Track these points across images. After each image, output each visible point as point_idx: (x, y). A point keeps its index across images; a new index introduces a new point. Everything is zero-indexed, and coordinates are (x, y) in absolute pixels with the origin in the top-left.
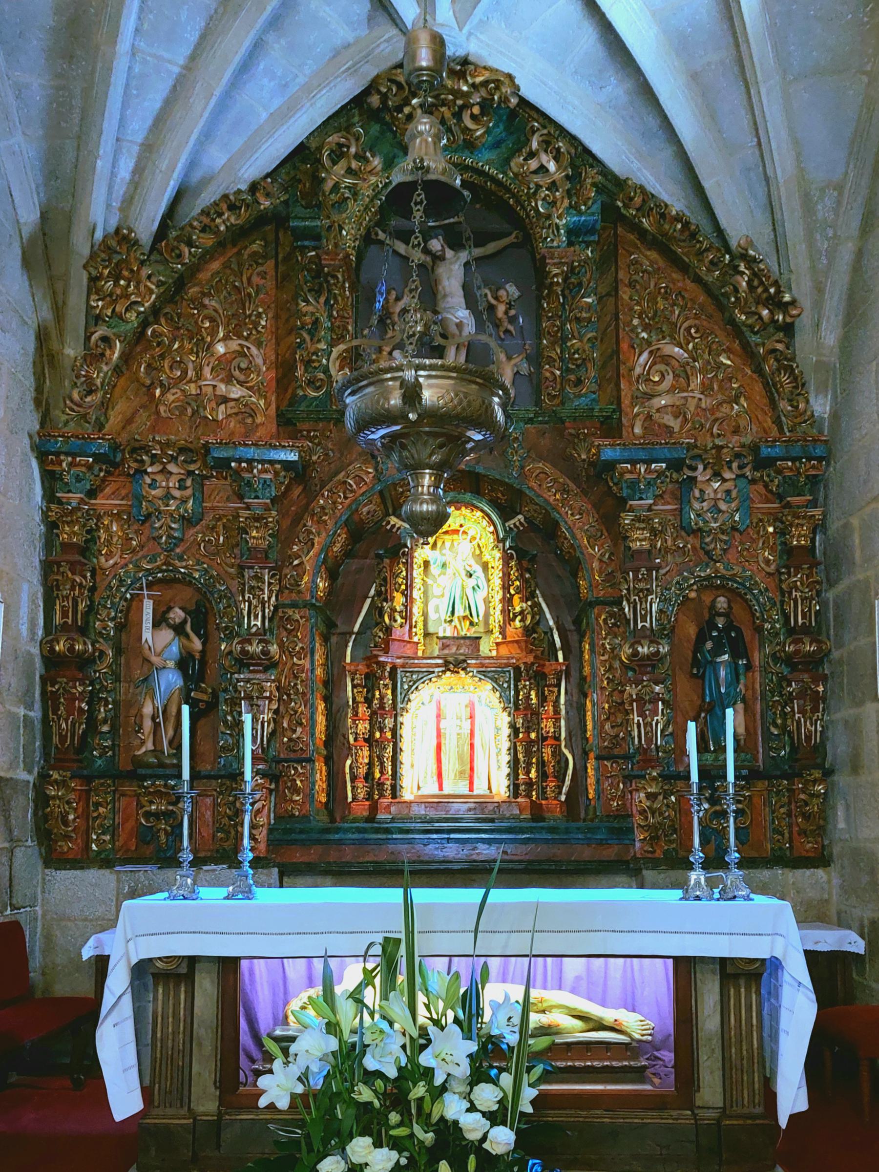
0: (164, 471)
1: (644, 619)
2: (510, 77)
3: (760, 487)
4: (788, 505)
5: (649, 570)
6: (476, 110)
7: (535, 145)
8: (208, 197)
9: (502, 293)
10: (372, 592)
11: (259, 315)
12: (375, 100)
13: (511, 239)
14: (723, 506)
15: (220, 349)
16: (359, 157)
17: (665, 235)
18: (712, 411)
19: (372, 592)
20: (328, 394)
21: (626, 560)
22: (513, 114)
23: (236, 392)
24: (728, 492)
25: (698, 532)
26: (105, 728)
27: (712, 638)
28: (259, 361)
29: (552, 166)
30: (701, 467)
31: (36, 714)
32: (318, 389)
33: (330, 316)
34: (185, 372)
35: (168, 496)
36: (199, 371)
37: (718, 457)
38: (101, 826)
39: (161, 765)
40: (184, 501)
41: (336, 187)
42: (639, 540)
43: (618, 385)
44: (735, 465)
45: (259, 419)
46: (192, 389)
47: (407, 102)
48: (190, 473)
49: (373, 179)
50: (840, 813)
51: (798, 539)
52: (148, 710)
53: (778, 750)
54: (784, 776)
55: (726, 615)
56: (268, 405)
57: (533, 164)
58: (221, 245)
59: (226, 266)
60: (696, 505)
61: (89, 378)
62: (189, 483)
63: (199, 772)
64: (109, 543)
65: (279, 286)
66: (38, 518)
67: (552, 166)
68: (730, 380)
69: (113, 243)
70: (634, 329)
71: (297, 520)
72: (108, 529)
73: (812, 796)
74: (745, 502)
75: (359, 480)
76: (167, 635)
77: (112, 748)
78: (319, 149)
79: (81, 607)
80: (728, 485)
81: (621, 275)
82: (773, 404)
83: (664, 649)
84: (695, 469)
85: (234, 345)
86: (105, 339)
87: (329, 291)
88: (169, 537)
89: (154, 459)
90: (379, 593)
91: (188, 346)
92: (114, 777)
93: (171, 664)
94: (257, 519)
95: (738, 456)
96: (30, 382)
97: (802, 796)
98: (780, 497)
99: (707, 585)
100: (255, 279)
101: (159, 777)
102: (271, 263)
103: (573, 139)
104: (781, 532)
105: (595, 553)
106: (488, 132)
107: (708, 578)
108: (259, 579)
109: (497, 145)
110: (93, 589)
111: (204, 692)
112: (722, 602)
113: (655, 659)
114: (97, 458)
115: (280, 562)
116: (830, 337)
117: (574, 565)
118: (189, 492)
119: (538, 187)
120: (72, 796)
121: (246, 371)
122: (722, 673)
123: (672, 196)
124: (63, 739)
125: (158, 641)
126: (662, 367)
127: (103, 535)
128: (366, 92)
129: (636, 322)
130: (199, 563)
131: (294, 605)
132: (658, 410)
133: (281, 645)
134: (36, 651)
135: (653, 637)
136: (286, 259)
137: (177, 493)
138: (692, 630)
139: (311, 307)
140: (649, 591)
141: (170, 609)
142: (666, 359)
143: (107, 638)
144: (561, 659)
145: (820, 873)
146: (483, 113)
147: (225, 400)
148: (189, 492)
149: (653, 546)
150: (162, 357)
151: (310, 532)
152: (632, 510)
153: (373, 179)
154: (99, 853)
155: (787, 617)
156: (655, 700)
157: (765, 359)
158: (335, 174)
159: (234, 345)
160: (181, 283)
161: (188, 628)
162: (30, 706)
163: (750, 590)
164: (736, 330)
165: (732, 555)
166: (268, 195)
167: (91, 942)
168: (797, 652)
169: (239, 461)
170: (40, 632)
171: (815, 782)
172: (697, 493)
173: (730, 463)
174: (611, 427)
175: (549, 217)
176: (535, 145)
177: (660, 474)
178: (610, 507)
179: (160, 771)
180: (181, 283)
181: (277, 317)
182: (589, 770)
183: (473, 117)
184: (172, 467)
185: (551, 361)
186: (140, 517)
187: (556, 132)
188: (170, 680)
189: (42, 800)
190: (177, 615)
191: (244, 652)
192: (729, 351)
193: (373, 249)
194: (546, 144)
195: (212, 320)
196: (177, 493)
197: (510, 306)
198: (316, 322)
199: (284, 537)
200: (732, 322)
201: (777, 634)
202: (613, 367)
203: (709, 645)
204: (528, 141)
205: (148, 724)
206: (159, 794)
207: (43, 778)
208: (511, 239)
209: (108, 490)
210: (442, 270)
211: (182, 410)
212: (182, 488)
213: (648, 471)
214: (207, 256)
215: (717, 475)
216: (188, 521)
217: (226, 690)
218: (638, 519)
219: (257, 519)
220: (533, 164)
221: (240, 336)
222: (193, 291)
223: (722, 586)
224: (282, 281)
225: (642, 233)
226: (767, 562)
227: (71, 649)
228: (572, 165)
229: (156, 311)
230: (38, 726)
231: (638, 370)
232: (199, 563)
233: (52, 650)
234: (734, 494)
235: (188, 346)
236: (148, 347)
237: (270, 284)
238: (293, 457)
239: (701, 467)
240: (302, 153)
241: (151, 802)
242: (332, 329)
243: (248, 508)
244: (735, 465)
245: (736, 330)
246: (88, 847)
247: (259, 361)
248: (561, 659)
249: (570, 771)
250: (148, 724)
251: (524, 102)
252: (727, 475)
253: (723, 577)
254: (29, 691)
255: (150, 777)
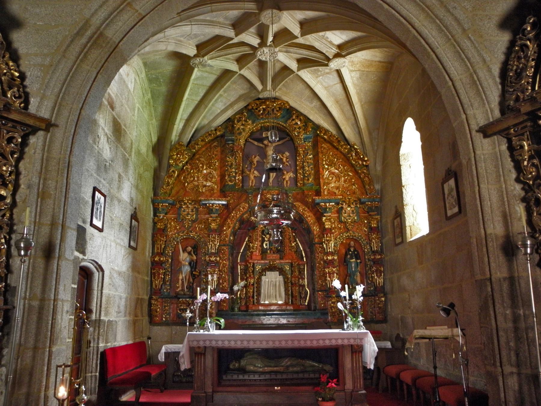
0: (188, 207)
1: (329, 249)
2: (287, 102)
3: (362, 209)
4: (370, 215)
5: (331, 234)
6: (278, 109)
7: (294, 117)
8: (203, 132)
9: (284, 155)
10: (247, 239)
11: (216, 162)
12: (250, 107)
13: (287, 139)
14: (351, 215)
15: (205, 172)
16: (246, 121)
17: (331, 141)
18: (347, 188)
19: (247, 239)
20: (235, 183)
21: (324, 231)
22: (288, 109)
23: (209, 184)
24: (353, 211)
25: (345, 223)
26: (168, 283)
27: (349, 254)
28: (215, 175)
29: (299, 123)
30: (344, 204)
31: (149, 279)
32: (232, 182)
33: (236, 162)
34: (194, 179)
35: (188, 214)
36: (198, 177)
37: (349, 201)
38: (166, 313)
39: (184, 294)
40: (193, 215)
41: (239, 129)
42: (327, 225)
43: (319, 180)
44: (354, 203)
45: (215, 191)
46: (196, 183)
47: (259, 107)
48: (195, 207)
49: (249, 127)
50: (389, 307)
51: (374, 225)
52: (181, 277)
53: (370, 288)
54: (372, 296)
55: (354, 247)
56: (217, 187)
57: (294, 122)
58: (206, 144)
59: (207, 149)
60: (344, 215)
61: (168, 182)
62: (194, 210)
63: (523, 189)
64: (170, 227)
65: (222, 154)
66: (151, 221)
67: (299, 123)
68: (352, 179)
69: (177, 146)
70: (324, 165)
71: (226, 220)
72: (170, 224)
73: (381, 301)
74: (358, 215)
75: (244, 208)
76: (186, 255)
77: (170, 289)
78: (234, 119)
79: (163, 246)
80: (353, 209)
81: (319, 150)
82: (364, 187)
83: (336, 258)
84: (343, 205)
85: (208, 171)
86: (173, 171)
87: (236, 155)
88: (188, 226)
89: (185, 204)
90: (249, 241)
91: (195, 171)
92: (170, 298)
93: (187, 263)
94: (214, 220)
95: (355, 201)
96: (152, 184)
97: (378, 302)
98: (368, 212)
99: (348, 238)
100: (215, 153)
101: (184, 298)
102: (219, 148)
103: (305, 116)
104: (369, 222)
105: (316, 229)
106: (281, 114)
107: (348, 236)
108: (214, 238)
109: (284, 117)
110: (166, 241)
111: (197, 272)
112: (352, 243)
113: (332, 261)
114: (169, 204)
115: (219, 231)
116: (379, 168)
117: (309, 231)
118: (194, 213)
119: (295, 128)
120: (159, 304)
121: (212, 178)
122: (353, 265)
123: (332, 130)
124: (156, 286)
125: (184, 257)
126: (332, 176)
127: (169, 226)
128: (248, 105)
129: (324, 163)
130: (196, 233)
131: (224, 245)
132: (331, 188)
133: (220, 258)
134: (150, 260)
135: (332, 254)
136: (223, 146)
137: (191, 213)
138: (344, 251)
139: (230, 159)
140: (331, 240)
141: (187, 247)
142: (333, 173)
143: (169, 256)
144: (305, 260)
145: (384, 325)
146: (280, 110)
147: (205, 186)
148: (194, 213)
149: (332, 226)
150: (188, 174)
151: (229, 224)
152: (325, 216)
153: (249, 127)
154: (165, 321)
155: (371, 248)
156: (333, 273)
157: (361, 174)
158: (238, 126)
159: (208, 171)
160: (194, 155)
161: (192, 253)
162: (148, 276)
163: (360, 239)
164: (352, 166)
165: (355, 229)
166: (220, 131)
167: (163, 348)
168: (375, 258)
169: (209, 204)
170: (151, 255)
171: (382, 297)
172: (344, 211)
173: (353, 203)
174: (318, 193)
175: (298, 136)
176: (294, 117)
177: (333, 206)
178: (319, 214)
179: (185, 296)
180: (194, 155)
181: (221, 162)
182: (425, 354)
183: (277, 111)
184: (190, 206)
185: (300, 173)
186: (180, 220)
187: (300, 114)
188: (186, 269)
189: (150, 304)
190: (189, 249)
191: (210, 260)
192: (351, 171)
193: (248, 143)
194: (297, 117)
195: (202, 164)
196: (191, 213)
197: (287, 158)
198: (232, 164)
199: (221, 226)
200: (352, 164)
201: (369, 253)
202: (318, 176)
203: (349, 256)
204: (292, 116)
205: (180, 282)
206: (184, 303)
207: (150, 298)
208: (287, 139)
209: (171, 212)
210: (268, 149)
211: (193, 189)
212: (192, 211)
213: (329, 205)
214: (203, 147)
215: (349, 206)
216: (193, 221)
217: (204, 271)
218: (326, 219)
219: (214, 220)
220: (294, 122)
221: (210, 168)
222: (197, 156)
223: (352, 238)
224: (222, 152)
225: (325, 140)
226: (365, 231)
227: (160, 260)
228: (305, 122)
229: (187, 163)
230: (149, 282)
231: (325, 176)
232: (196, 233)
233: (154, 260)
234: (355, 211)
235: (195, 171)
236: (184, 172)
237: (219, 153)
238: (224, 203)
239: (344, 204)
240: (230, 120)
241: (181, 306)
242: (236, 165)
243: (211, 217)
244: (354, 203)
245: (352, 166)
246: (162, 319)
247: (215, 175)
248: (305, 260)
249: (308, 295)
250: (180, 282)
251: (291, 107)
252: (352, 206)
253: (352, 236)
254: (148, 273)
255: (182, 298)
